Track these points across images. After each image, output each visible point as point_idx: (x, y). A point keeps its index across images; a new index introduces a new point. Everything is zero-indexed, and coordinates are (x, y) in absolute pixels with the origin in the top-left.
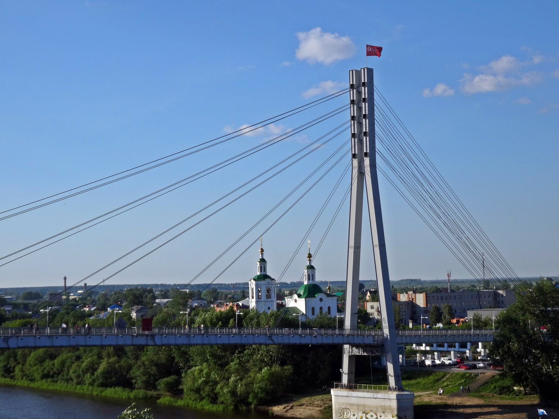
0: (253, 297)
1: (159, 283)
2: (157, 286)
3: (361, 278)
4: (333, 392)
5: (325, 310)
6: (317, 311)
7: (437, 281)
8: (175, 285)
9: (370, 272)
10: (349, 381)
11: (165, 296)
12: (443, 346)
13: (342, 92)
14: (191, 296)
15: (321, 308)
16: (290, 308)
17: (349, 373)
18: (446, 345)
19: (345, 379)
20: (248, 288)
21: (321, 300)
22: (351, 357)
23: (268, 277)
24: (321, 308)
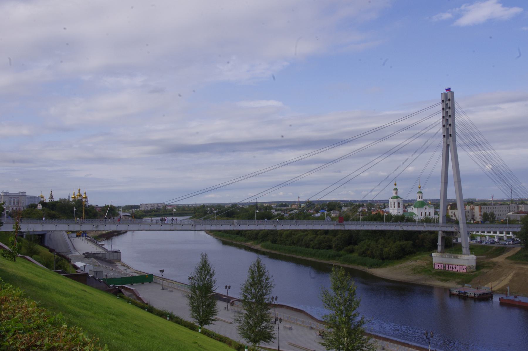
0: (394, 207)
1: (343, 199)
2: (342, 201)
3: (448, 197)
4: (434, 254)
5: (428, 214)
6: (424, 214)
7: (255, 206)
8: (351, 201)
9: (452, 195)
10: (442, 249)
11: (345, 206)
12: (509, 234)
13: (437, 105)
14: (359, 206)
15: (426, 213)
16: (56, 202)
17: (442, 245)
18: (504, 232)
19: (439, 248)
20: (389, 203)
21: (426, 208)
22: (442, 238)
23: (399, 197)
24: (426, 213)
